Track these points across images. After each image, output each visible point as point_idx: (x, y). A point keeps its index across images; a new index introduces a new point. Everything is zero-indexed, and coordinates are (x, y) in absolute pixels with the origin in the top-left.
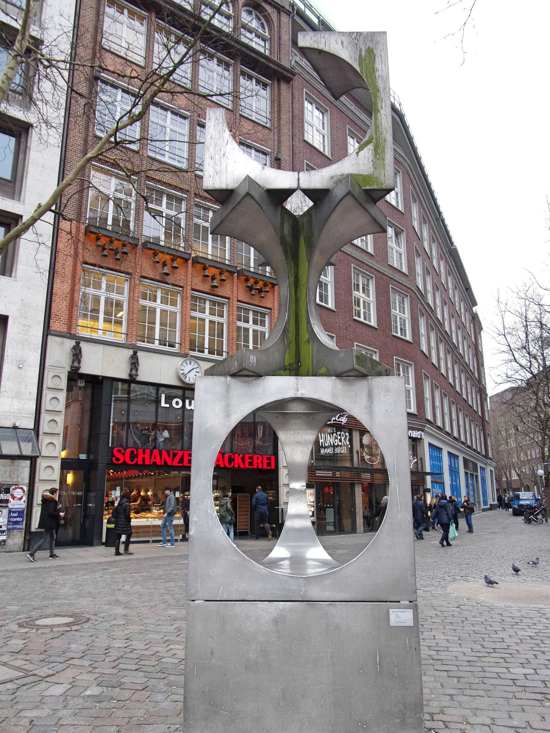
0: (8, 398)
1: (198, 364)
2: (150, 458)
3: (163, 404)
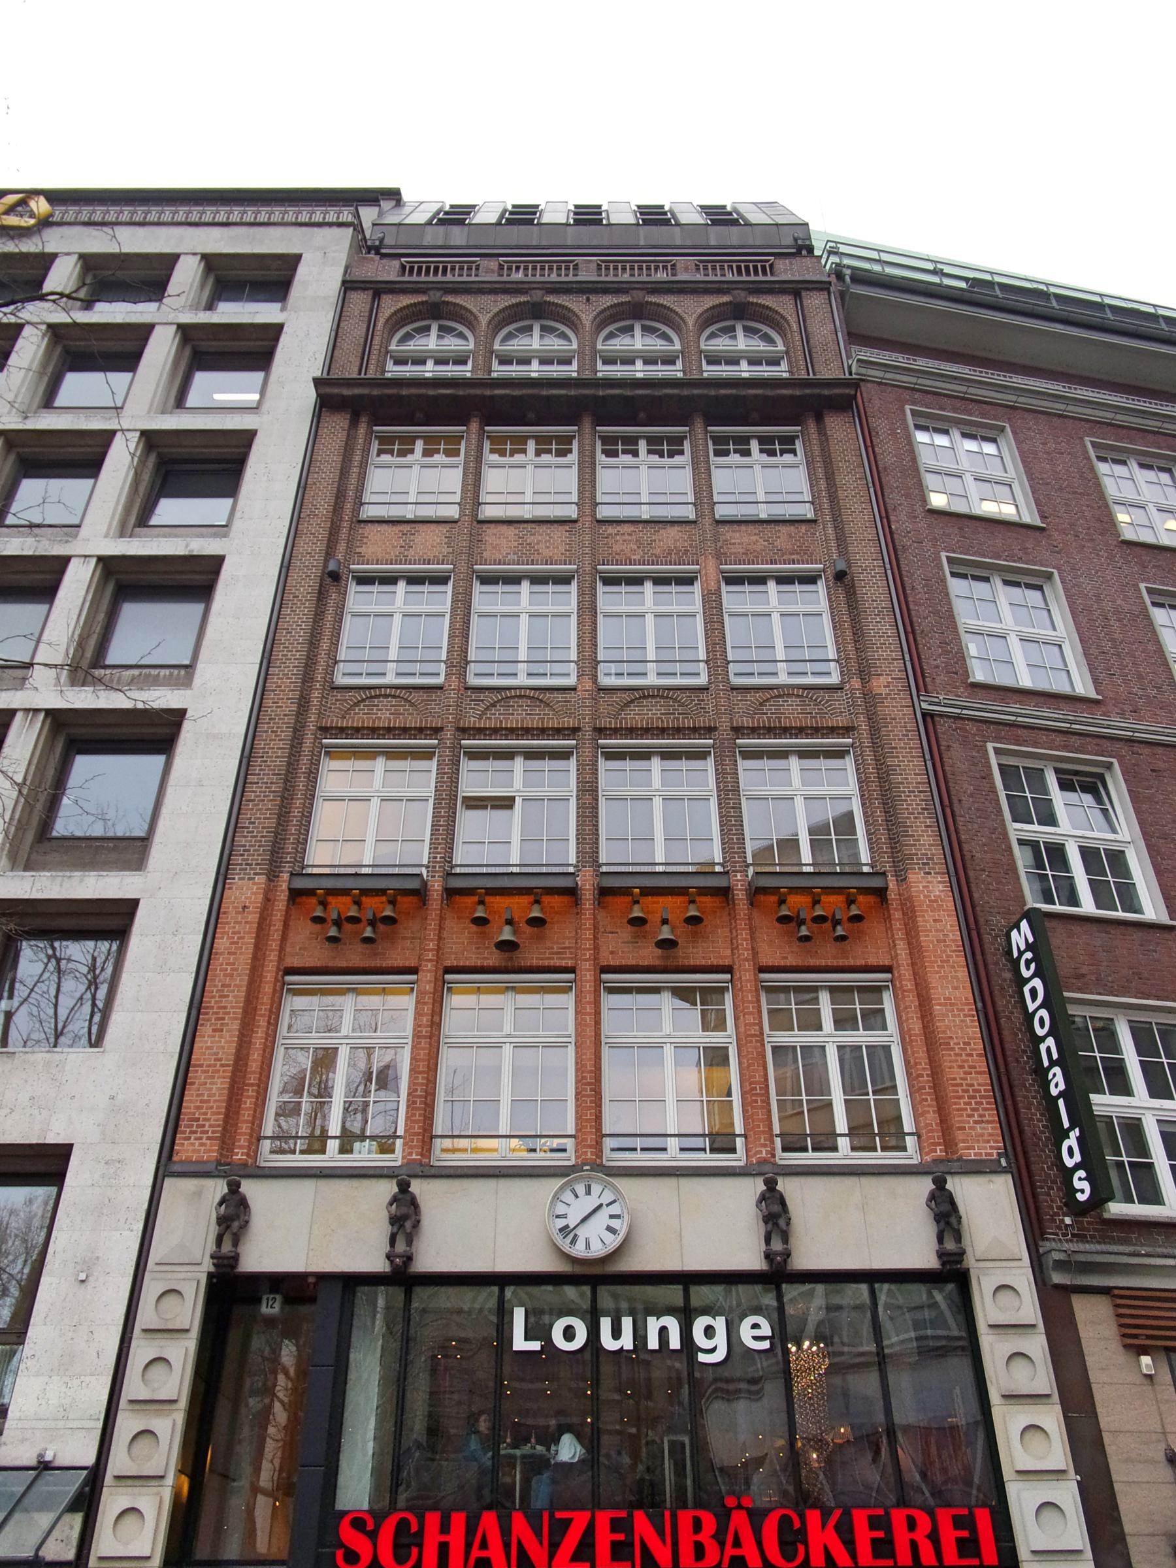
0: (38, 1374)
1: (615, 1189)
2: (469, 1545)
3: (520, 1343)
